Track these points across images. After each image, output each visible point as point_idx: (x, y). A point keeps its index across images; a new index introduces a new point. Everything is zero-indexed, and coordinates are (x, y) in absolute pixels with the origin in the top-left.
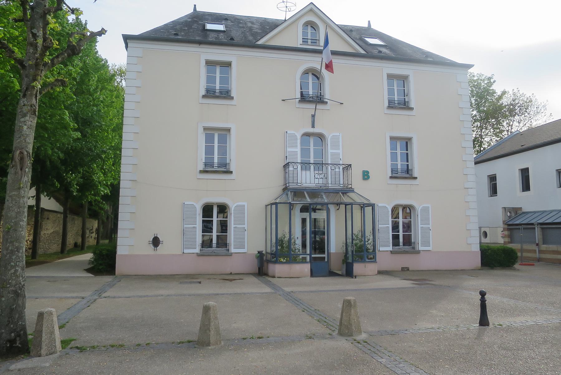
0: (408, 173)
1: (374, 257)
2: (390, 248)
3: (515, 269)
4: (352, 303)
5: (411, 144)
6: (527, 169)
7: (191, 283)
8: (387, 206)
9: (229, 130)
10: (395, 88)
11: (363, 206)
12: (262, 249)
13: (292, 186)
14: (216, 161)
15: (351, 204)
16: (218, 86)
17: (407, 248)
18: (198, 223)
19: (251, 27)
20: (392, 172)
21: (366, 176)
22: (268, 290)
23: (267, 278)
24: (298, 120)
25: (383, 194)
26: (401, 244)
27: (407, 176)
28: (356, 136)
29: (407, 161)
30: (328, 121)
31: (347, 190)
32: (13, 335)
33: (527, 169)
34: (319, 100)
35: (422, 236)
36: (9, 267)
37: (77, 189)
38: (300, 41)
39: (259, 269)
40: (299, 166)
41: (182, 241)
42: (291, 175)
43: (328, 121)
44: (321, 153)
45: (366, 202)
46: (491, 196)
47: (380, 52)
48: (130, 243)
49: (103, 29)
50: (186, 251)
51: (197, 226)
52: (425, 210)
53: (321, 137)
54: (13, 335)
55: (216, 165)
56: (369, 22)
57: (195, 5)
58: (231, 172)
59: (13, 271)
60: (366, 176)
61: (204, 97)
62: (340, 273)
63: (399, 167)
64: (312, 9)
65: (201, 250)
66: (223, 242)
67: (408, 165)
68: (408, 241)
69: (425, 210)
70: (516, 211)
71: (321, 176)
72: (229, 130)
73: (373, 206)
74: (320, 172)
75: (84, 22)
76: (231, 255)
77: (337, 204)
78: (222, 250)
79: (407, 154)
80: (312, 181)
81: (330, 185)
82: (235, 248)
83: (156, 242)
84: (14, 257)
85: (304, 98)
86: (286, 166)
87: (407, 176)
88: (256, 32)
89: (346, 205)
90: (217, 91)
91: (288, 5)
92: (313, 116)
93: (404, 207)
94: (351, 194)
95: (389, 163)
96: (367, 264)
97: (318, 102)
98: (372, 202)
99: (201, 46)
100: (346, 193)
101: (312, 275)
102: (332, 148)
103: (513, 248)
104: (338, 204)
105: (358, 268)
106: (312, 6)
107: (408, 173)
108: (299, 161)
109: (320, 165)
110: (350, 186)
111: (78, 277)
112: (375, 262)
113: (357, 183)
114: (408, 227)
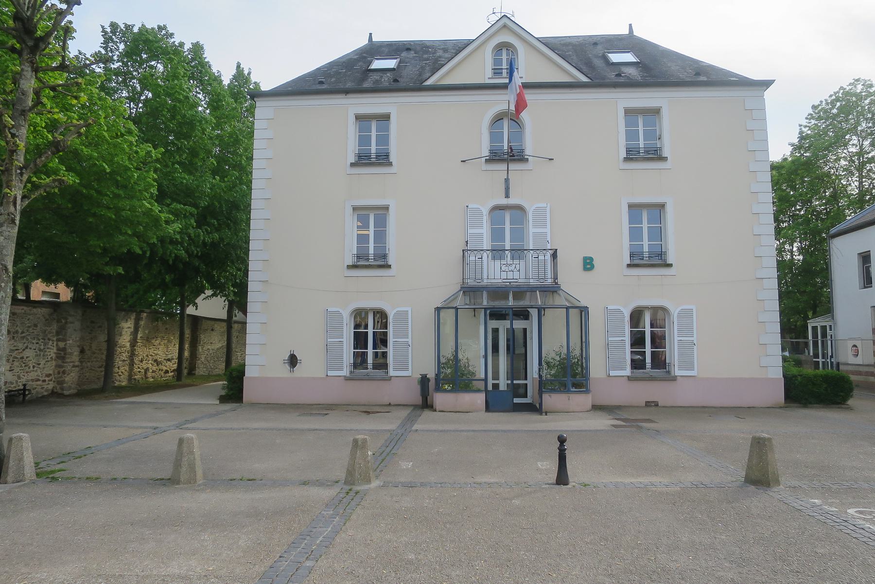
2: (628, 371)
3: (850, 409)
4: (360, 443)
7: (311, 414)
8: (341, 311)
9: (386, 208)
10: (641, 129)
14: (371, 251)
16: (373, 149)
17: (657, 372)
18: (345, 336)
21: (588, 264)
24: (485, 188)
26: (370, 366)
28: (576, 203)
31: (553, 289)
34: (515, 156)
35: (680, 355)
37: (234, 292)
38: (489, 73)
41: (326, 361)
42: (472, 266)
43: (529, 187)
44: (519, 233)
46: (865, 287)
48: (260, 361)
50: (330, 373)
51: (344, 340)
52: (686, 314)
53: (520, 208)
56: (630, 25)
57: (371, 34)
60: (588, 264)
64: (505, 24)
65: (351, 372)
66: (381, 364)
68: (659, 362)
69: (686, 314)
72: (386, 208)
73: (584, 311)
75: (246, 72)
78: (379, 373)
80: (498, 276)
81: (531, 281)
83: (293, 361)
87: (660, 262)
93: (655, 310)
97: (511, 160)
98: (583, 303)
99: (349, 96)
101: (488, 408)
102: (534, 226)
106: (505, 20)
108: (508, 247)
109: (518, 252)
111: (188, 404)
112: (587, 391)
114: (658, 341)
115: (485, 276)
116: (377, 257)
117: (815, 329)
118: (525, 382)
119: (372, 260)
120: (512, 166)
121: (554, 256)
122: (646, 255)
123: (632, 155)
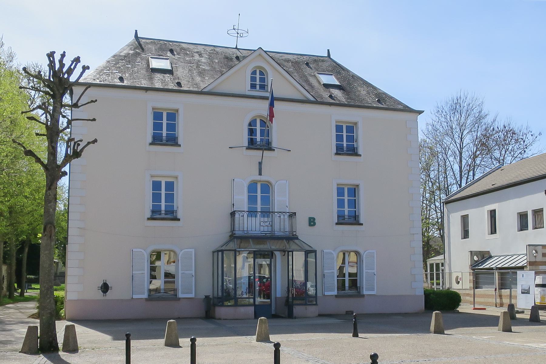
6: (495, 211)
8: (333, 252)
12: (209, 293)
13: (238, 233)
14: (163, 208)
21: (312, 222)
24: (244, 166)
25: (329, 241)
31: (292, 238)
32: (51, 339)
33: (495, 211)
34: (268, 146)
39: (206, 312)
40: (246, 215)
43: (275, 167)
44: (266, 200)
45: (310, 249)
50: (135, 297)
55: (163, 212)
56: (328, 50)
57: (136, 31)
58: (179, 220)
59: (48, 301)
60: (312, 222)
61: (151, 144)
62: (283, 315)
70: (485, 256)
71: (266, 224)
73: (315, 252)
74: (266, 219)
76: (179, 299)
82: (183, 293)
83: (105, 288)
85: (252, 144)
86: (233, 214)
88: (204, 70)
90: (164, 138)
92: (260, 164)
96: (307, 307)
97: (265, 149)
98: (315, 247)
105: (298, 310)
112: (316, 304)
116: (167, 212)
117: (432, 265)
118: (432, 328)
119: (164, 211)
120: (264, 151)
121: (292, 215)
122: (346, 217)
123: (157, 140)
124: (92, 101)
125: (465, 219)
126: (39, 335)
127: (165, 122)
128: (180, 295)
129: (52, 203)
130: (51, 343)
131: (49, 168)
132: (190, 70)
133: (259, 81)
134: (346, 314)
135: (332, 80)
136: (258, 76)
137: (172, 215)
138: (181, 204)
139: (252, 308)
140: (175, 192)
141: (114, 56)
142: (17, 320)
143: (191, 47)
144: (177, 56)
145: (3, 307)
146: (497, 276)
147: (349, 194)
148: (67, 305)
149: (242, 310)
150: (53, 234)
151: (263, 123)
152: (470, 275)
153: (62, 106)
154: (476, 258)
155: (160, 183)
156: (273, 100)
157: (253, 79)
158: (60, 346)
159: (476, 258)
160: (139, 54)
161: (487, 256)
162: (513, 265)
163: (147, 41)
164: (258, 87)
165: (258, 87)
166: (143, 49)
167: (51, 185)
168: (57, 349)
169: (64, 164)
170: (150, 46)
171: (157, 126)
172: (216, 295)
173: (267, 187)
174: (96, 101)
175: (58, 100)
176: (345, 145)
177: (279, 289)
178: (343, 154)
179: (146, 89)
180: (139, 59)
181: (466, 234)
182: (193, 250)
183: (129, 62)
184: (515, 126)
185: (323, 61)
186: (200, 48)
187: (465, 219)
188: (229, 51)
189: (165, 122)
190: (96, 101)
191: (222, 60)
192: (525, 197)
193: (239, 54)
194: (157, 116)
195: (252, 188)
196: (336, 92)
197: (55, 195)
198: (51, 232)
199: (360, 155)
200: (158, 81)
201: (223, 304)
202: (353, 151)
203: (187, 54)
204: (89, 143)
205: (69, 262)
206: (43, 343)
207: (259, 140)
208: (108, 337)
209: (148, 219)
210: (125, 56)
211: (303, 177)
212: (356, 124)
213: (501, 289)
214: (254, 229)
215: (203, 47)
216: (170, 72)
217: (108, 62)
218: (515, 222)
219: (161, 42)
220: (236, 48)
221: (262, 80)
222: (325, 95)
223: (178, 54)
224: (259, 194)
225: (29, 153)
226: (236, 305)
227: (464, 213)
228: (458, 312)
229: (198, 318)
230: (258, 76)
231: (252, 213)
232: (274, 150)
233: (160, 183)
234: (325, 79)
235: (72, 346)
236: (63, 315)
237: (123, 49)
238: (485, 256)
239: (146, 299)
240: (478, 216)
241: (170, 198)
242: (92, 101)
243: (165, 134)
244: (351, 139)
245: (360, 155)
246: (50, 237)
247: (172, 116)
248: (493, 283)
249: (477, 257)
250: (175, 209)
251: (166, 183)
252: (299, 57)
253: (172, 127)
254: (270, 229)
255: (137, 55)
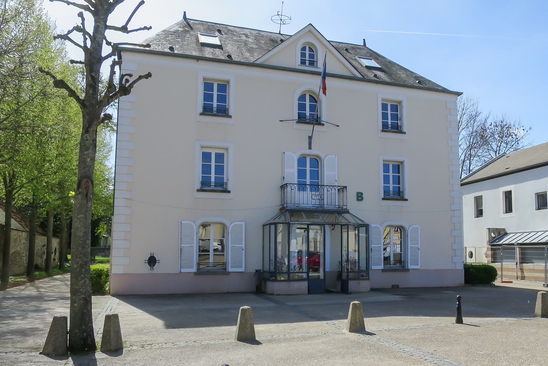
0: (399, 195)
1: (368, 275)
5: (403, 167)
8: (380, 227)
11: (357, 227)
12: (260, 267)
13: (290, 206)
14: (213, 180)
15: (348, 225)
19: (246, 41)
20: (384, 194)
21: (360, 197)
22: (272, 305)
23: (266, 295)
24: (294, 141)
27: (399, 197)
29: (399, 184)
30: (325, 143)
32: (85, 334)
34: (316, 121)
36: (80, 279)
43: (325, 143)
44: (315, 174)
47: (375, 76)
49: (149, 73)
50: (183, 270)
54: (85, 334)
55: (213, 184)
56: (364, 40)
57: (185, 12)
58: (229, 192)
59: (82, 282)
60: (360, 197)
61: (201, 114)
63: (391, 189)
64: (310, 29)
67: (399, 187)
70: (501, 233)
73: (367, 226)
74: (317, 193)
76: (229, 273)
77: (333, 225)
79: (399, 176)
83: (152, 261)
84: (83, 270)
85: (302, 119)
86: (283, 187)
87: (399, 197)
89: (342, 225)
90: (215, 109)
91: (283, 18)
92: (310, 138)
94: (346, 216)
95: (382, 184)
97: (316, 124)
98: (367, 222)
100: (341, 214)
103: (495, 267)
104: (333, 225)
105: (352, 285)
107: (399, 195)
109: (316, 186)
110: (345, 207)
112: (368, 279)
113: (352, 204)
115: (325, 203)
120: (315, 126)
123: (207, 110)
124: (145, 28)
125: (478, 201)
126: (68, 329)
127: (215, 93)
128: (230, 269)
129: (90, 151)
130: (85, 340)
131: (87, 104)
132: (238, 47)
133: (309, 56)
134: (392, 288)
135: (373, 63)
136: (307, 52)
137: (221, 187)
138: (231, 176)
139: (306, 284)
140: (225, 164)
141: (164, 31)
142: (58, 295)
143: (238, 30)
144: (224, 36)
145: (50, 278)
146: (518, 251)
147: (395, 170)
148: (111, 279)
149: (296, 285)
150: (90, 193)
151: (313, 99)
152: (488, 250)
153: (107, 27)
154: (493, 235)
155: (210, 154)
156: (325, 75)
157: (303, 55)
158: (98, 338)
159: (493, 235)
160: (188, 31)
161: (502, 233)
162: (520, 242)
163: (196, 22)
164: (307, 63)
165: (307, 63)
166: (192, 28)
167: (89, 126)
168: (92, 348)
169: (108, 100)
170: (198, 26)
171: (208, 97)
172: (267, 268)
173: (316, 161)
174: (151, 28)
175: (102, 17)
176: (390, 123)
177: (330, 263)
178: (389, 132)
179: (198, 59)
180: (188, 35)
181: (479, 213)
182: (243, 223)
183: (179, 37)
184: (509, 120)
185: (360, 49)
186: (247, 32)
187: (478, 201)
188: (274, 36)
189: (215, 93)
190: (151, 28)
191: (268, 42)
192: (544, 179)
193: (282, 38)
194: (208, 86)
195: (302, 161)
196: (379, 73)
197: (95, 140)
198: (87, 188)
199: (405, 133)
200: (208, 53)
201: (276, 278)
202: (397, 129)
203: (234, 35)
204: (140, 77)
205: (115, 234)
206: (75, 339)
207: (309, 114)
208: (159, 323)
209: (198, 190)
210: (175, 32)
211: (351, 156)
212: (400, 102)
213: (522, 263)
214: (305, 202)
215: (249, 30)
216: (220, 47)
217: (158, 35)
218: (533, 202)
219: (209, 24)
220: (280, 33)
221: (312, 56)
222: (370, 75)
223: (226, 34)
224: (308, 168)
225: (60, 84)
226: (289, 280)
227: (507, 188)
228: (494, 286)
229: (248, 292)
230: (307, 52)
231: (302, 186)
232: (323, 125)
233: (210, 154)
234: (366, 62)
235: (114, 347)
236: (107, 289)
237: (173, 26)
238: (501, 233)
239: (195, 273)
240: (493, 198)
241: (220, 170)
242: (145, 28)
243: (216, 105)
244: (395, 117)
245: (405, 133)
246: (87, 195)
247: (223, 87)
248: (514, 258)
249: (494, 234)
250: (225, 181)
251: (217, 154)
252: (338, 44)
253: (222, 98)
254: (317, 202)
255: (186, 32)
